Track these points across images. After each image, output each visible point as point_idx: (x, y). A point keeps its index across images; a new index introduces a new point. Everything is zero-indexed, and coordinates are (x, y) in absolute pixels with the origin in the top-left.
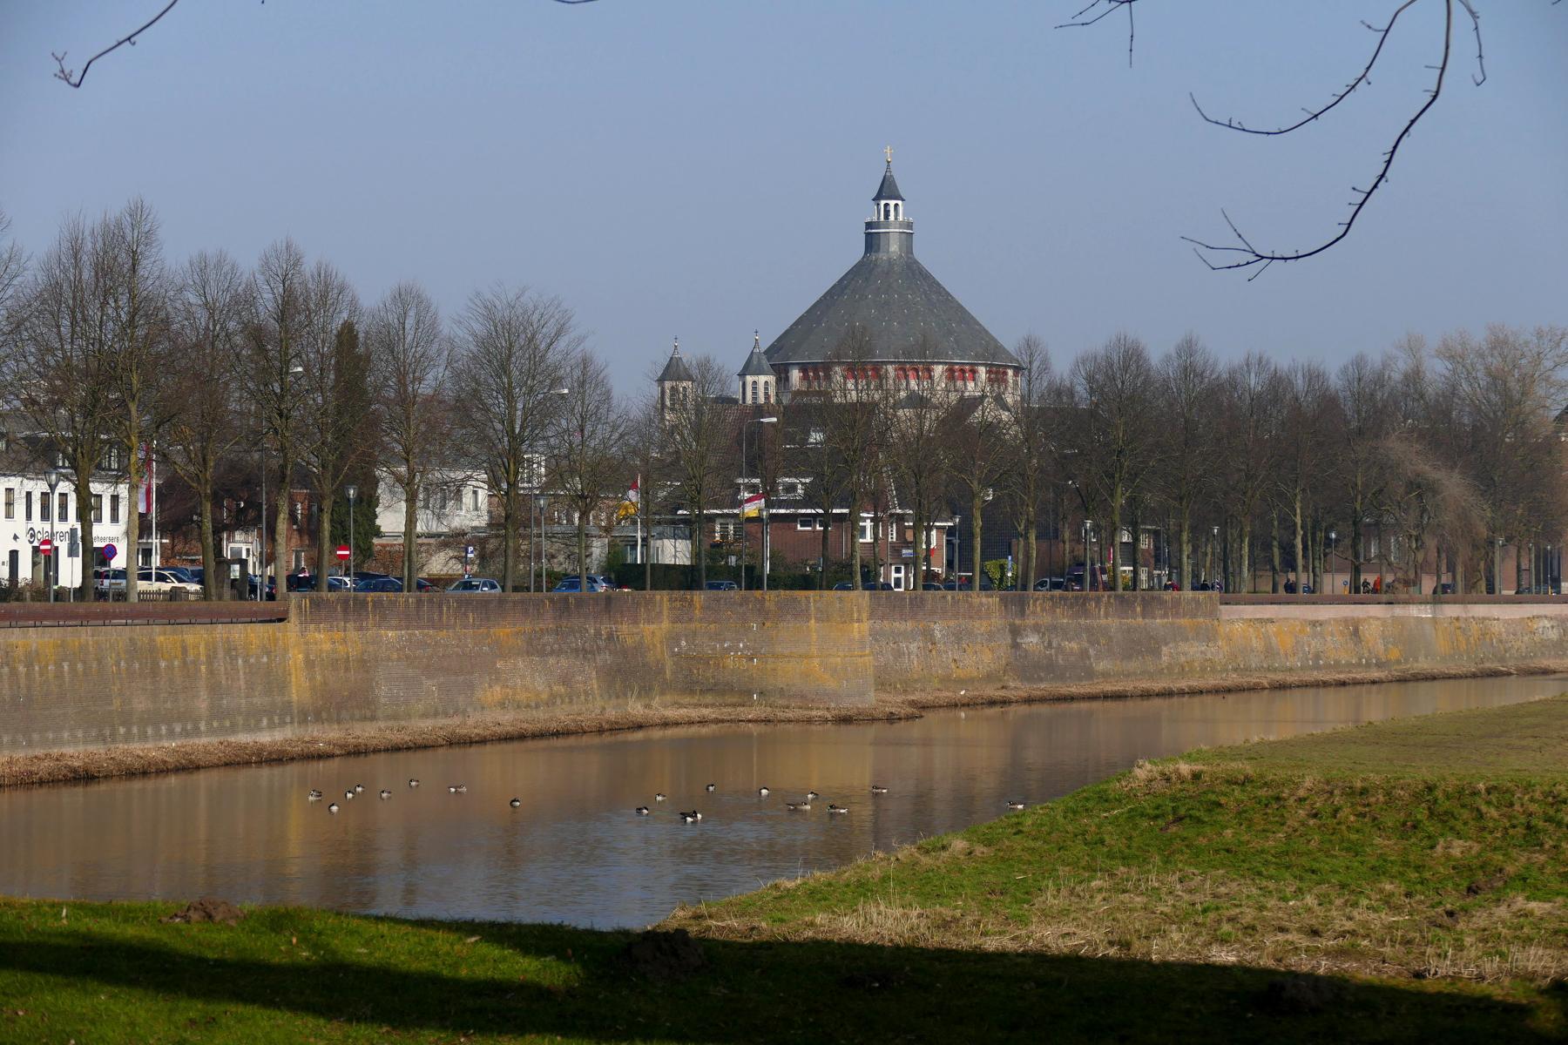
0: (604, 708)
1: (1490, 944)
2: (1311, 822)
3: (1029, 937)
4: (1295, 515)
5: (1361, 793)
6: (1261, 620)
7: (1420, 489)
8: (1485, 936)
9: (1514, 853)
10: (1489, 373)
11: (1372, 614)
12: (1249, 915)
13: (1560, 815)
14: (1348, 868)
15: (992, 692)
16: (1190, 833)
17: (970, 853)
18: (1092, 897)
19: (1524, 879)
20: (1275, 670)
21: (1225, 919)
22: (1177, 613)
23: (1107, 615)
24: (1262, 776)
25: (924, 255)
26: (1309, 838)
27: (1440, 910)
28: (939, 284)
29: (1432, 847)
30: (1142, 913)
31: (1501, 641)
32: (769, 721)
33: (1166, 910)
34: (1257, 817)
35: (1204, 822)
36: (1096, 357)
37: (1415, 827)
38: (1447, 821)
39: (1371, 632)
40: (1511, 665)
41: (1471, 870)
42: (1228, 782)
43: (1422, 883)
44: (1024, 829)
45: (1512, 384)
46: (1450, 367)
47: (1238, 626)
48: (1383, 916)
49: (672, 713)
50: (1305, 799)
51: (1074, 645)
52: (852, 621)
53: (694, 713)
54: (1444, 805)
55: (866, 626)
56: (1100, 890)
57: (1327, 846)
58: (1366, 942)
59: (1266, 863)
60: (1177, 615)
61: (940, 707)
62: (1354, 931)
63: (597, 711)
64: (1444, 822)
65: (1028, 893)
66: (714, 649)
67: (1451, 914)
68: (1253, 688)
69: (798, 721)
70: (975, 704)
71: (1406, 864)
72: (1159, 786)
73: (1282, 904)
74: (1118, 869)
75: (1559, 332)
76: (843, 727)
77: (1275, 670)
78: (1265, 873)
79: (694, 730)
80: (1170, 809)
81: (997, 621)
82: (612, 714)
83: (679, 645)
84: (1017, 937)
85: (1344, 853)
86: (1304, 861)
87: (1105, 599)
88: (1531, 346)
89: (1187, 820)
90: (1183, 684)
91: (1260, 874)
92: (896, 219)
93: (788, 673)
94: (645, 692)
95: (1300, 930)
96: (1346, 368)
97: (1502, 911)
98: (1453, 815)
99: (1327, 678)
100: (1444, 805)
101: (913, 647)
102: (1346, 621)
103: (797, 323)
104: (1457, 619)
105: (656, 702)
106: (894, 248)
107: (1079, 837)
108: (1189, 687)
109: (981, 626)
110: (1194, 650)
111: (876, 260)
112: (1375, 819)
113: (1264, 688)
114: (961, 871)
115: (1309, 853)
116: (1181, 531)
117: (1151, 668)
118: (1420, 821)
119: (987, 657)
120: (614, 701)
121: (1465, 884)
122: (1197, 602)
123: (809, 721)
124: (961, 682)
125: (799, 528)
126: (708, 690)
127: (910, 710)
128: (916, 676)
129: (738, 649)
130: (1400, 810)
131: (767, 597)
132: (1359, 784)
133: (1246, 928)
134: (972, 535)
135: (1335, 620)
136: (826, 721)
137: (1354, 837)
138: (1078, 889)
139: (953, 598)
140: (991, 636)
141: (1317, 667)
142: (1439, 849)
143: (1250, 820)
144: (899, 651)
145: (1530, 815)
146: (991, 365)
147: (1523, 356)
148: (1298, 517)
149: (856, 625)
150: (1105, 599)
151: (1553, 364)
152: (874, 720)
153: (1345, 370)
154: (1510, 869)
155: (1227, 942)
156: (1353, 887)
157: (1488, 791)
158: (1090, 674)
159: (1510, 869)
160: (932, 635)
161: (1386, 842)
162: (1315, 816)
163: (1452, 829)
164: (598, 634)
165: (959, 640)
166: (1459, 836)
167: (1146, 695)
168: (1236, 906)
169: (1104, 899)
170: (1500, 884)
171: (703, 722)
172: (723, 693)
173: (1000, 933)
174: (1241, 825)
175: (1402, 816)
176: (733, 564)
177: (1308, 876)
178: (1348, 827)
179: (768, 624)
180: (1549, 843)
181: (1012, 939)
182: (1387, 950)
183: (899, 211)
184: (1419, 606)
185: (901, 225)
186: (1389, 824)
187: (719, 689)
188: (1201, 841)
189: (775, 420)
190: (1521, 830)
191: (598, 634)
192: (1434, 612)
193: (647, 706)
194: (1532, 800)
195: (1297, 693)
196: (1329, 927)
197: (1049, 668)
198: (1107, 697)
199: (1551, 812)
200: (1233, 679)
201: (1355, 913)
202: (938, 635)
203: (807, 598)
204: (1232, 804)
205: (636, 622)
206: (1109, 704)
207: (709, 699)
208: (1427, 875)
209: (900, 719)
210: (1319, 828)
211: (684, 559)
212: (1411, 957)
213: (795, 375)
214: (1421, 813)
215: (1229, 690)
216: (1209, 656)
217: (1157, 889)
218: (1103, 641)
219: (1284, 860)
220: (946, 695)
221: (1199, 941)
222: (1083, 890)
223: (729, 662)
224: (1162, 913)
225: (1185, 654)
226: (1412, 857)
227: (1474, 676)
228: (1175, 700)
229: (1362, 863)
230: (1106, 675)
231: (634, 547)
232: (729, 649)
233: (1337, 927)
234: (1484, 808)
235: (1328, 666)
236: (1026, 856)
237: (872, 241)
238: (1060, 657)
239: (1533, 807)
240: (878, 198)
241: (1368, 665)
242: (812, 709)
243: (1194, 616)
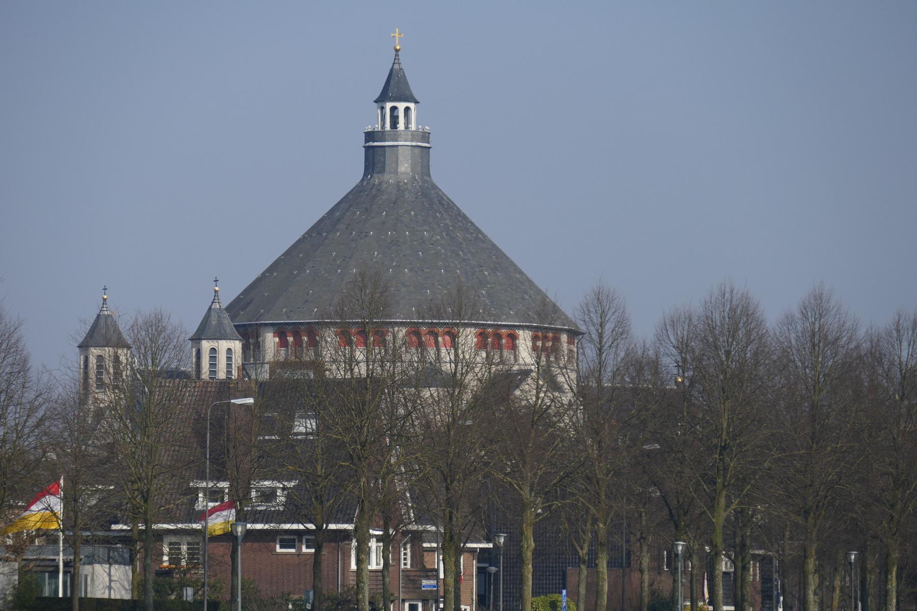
92: (407, 127)
103: (271, 269)
106: (404, 167)
111: (380, 184)
134: (520, 560)
185: (414, 136)
189: (250, 401)
211: (121, 592)
213: (270, 340)
231: (54, 573)
240: (381, 99)
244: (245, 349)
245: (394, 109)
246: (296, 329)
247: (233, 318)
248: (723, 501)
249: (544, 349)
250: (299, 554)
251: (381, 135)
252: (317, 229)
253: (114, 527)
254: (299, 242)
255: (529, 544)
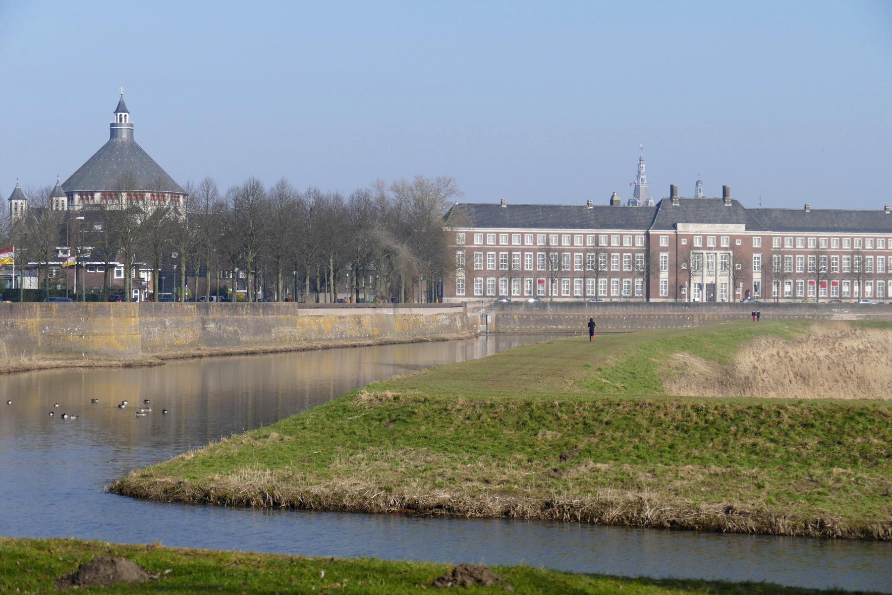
0: (9, 361)
1: (582, 487)
2: (467, 422)
3: (335, 486)
4: (330, 265)
5: (491, 407)
6: (316, 316)
7: (389, 253)
8: (578, 482)
9: (581, 437)
10: (415, 199)
11: (366, 313)
12: (449, 473)
13: (601, 418)
14: (493, 446)
15: (193, 351)
16: (402, 428)
17: (282, 440)
18: (359, 463)
19: (590, 452)
20: (323, 340)
21: (436, 475)
22: (279, 313)
23: (246, 314)
24: (433, 398)
25: (137, 139)
26: (468, 430)
27: (549, 468)
28: (146, 154)
29: (536, 435)
30: (390, 472)
31: (423, 325)
32: (91, 367)
33: (402, 470)
34: (437, 420)
35: (407, 422)
36: (238, 188)
37: (524, 424)
38: (541, 421)
39: (366, 321)
40: (428, 337)
41: (559, 447)
42: (414, 401)
43: (535, 454)
44: (307, 426)
45: (426, 203)
46: (397, 195)
47: (306, 319)
48: (521, 473)
49: (42, 363)
50: (461, 410)
51: (231, 329)
52: (131, 317)
53: (54, 363)
54: (537, 413)
55: (138, 319)
56: (363, 459)
57: (479, 434)
58: (516, 486)
59: (448, 444)
60: (279, 314)
61: (170, 359)
62: (508, 480)
63: (7, 362)
64: (539, 422)
65: (324, 461)
66: (62, 331)
67: (555, 470)
68: (314, 349)
69: (105, 367)
70: (187, 357)
71: (524, 443)
72: (376, 403)
73: (464, 466)
74: (369, 448)
75: (447, 179)
76: (127, 369)
77: (323, 340)
78: (449, 449)
79: (54, 371)
80: (386, 415)
81: (195, 317)
82: (13, 364)
83: (45, 330)
84: (328, 486)
85: (488, 438)
86: (468, 442)
87: (246, 306)
88: (435, 186)
89: (398, 422)
90: (282, 347)
91: (446, 449)
92: (125, 122)
93: (99, 343)
94: (29, 353)
95: (478, 480)
96: (353, 195)
97: (583, 469)
98: (543, 418)
99: (347, 343)
100: (537, 413)
101: (156, 330)
102: (355, 316)
103: (77, 172)
104: (404, 315)
105: (34, 357)
106: (125, 136)
107: (340, 431)
108: (285, 348)
109: (187, 319)
110: (286, 330)
111: (116, 141)
112: (501, 420)
113: (319, 349)
114: (281, 449)
115: (470, 438)
116: (278, 273)
117: (267, 339)
118: (526, 421)
119: (191, 334)
120: (14, 358)
121: (559, 454)
122: (288, 307)
123: (111, 366)
124: (180, 347)
125: (88, 271)
126: (59, 352)
127: (159, 361)
128: (157, 344)
129: (75, 331)
130: (514, 415)
131: (89, 305)
132: (489, 402)
133: (450, 479)
134: (181, 275)
135: (350, 316)
136: (119, 366)
137: (492, 430)
138: (351, 458)
139: (175, 306)
140: (192, 324)
141: (341, 338)
142: (539, 435)
143: (434, 421)
144: (149, 332)
145: (585, 417)
146: (172, 193)
147: (431, 190)
148: (331, 266)
149: (133, 319)
150: (246, 306)
151: (444, 195)
152: (142, 366)
153: (352, 197)
154: (581, 446)
155: (442, 487)
156: (500, 456)
157: (560, 405)
158: (239, 342)
159: (581, 446)
160: (165, 324)
161: (510, 432)
162: (468, 419)
163: (544, 425)
164: (6, 324)
165: (177, 327)
166: (548, 428)
167: (266, 352)
168: (440, 467)
169: (367, 464)
170: (577, 454)
171: (58, 367)
172: (67, 353)
173: (317, 484)
174: (429, 424)
175: (515, 419)
176: (59, 289)
177: (473, 450)
178: (488, 424)
179: (90, 319)
180: (598, 432)
181: (325, 487)
182: (529, 490)
183: (127, 118)
184: (387, 309)
185: (128, 125)
186: (510, 423)
187: (65, 351)
188: (409, 432)
189: (83, 218)
190: (581, 426)
191: (6, 324)
192: (394, 312)
193: (30, 360)
194: (584, 410)
195: (333, 350)
196: (494, 478)
197: (220, 340)
198: (247, 354)
199: (596, 416)
200: (304, 344)
201: (506, 470)
202: (167, 323)
203: (110, 306)
204: (421, 413)
205: (24, 318)
206: (249, 357)
207: (60, 356)
208: (537, 449)
209: (155, 365)
210: (472, 425)
211: (34, 287)
212: (542, 494)
213: (77, 197)
214: (526, 417)
215: (303, 350)
216: (293, 333)
217: (394, 458)
218: (244, 326)
219: (457, 441)
220: (172, 353)
221: (427, 486)
222: (353, 459)
223: (71, 338)
224: (401, 472)
225: (282, 332)
226: (526, 440)
227: (412, 342)
228: (279, 355)
229: (500, 444)
230: (246, 343)
231: (11, 280)
232: (70, 331)
233: (498, 478)
234: (559, 414)
235: (347, 338)
236: (314, 441)
237: (114, 133)
238: (225, 334)
239: (586, 414)
240: (116, 112)
241: (365, 337)
242: (111, 361)
243: (286, 314)
244: (68, 200)
245: (121, 115)
246: (87, 194)
247: (64, 189)
248: (250, 254)
249: (175, 200)
250: (96, 273)
251: (116, 125)
252: (93, 158)
253: (29, 263)
254: (88, 162)
255: (184, 269)
